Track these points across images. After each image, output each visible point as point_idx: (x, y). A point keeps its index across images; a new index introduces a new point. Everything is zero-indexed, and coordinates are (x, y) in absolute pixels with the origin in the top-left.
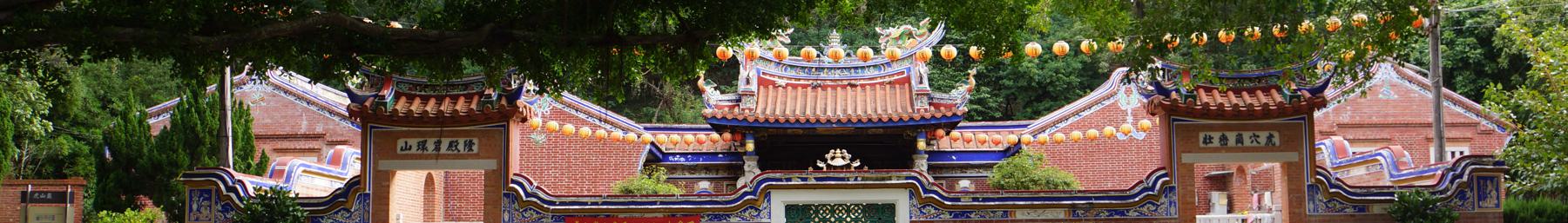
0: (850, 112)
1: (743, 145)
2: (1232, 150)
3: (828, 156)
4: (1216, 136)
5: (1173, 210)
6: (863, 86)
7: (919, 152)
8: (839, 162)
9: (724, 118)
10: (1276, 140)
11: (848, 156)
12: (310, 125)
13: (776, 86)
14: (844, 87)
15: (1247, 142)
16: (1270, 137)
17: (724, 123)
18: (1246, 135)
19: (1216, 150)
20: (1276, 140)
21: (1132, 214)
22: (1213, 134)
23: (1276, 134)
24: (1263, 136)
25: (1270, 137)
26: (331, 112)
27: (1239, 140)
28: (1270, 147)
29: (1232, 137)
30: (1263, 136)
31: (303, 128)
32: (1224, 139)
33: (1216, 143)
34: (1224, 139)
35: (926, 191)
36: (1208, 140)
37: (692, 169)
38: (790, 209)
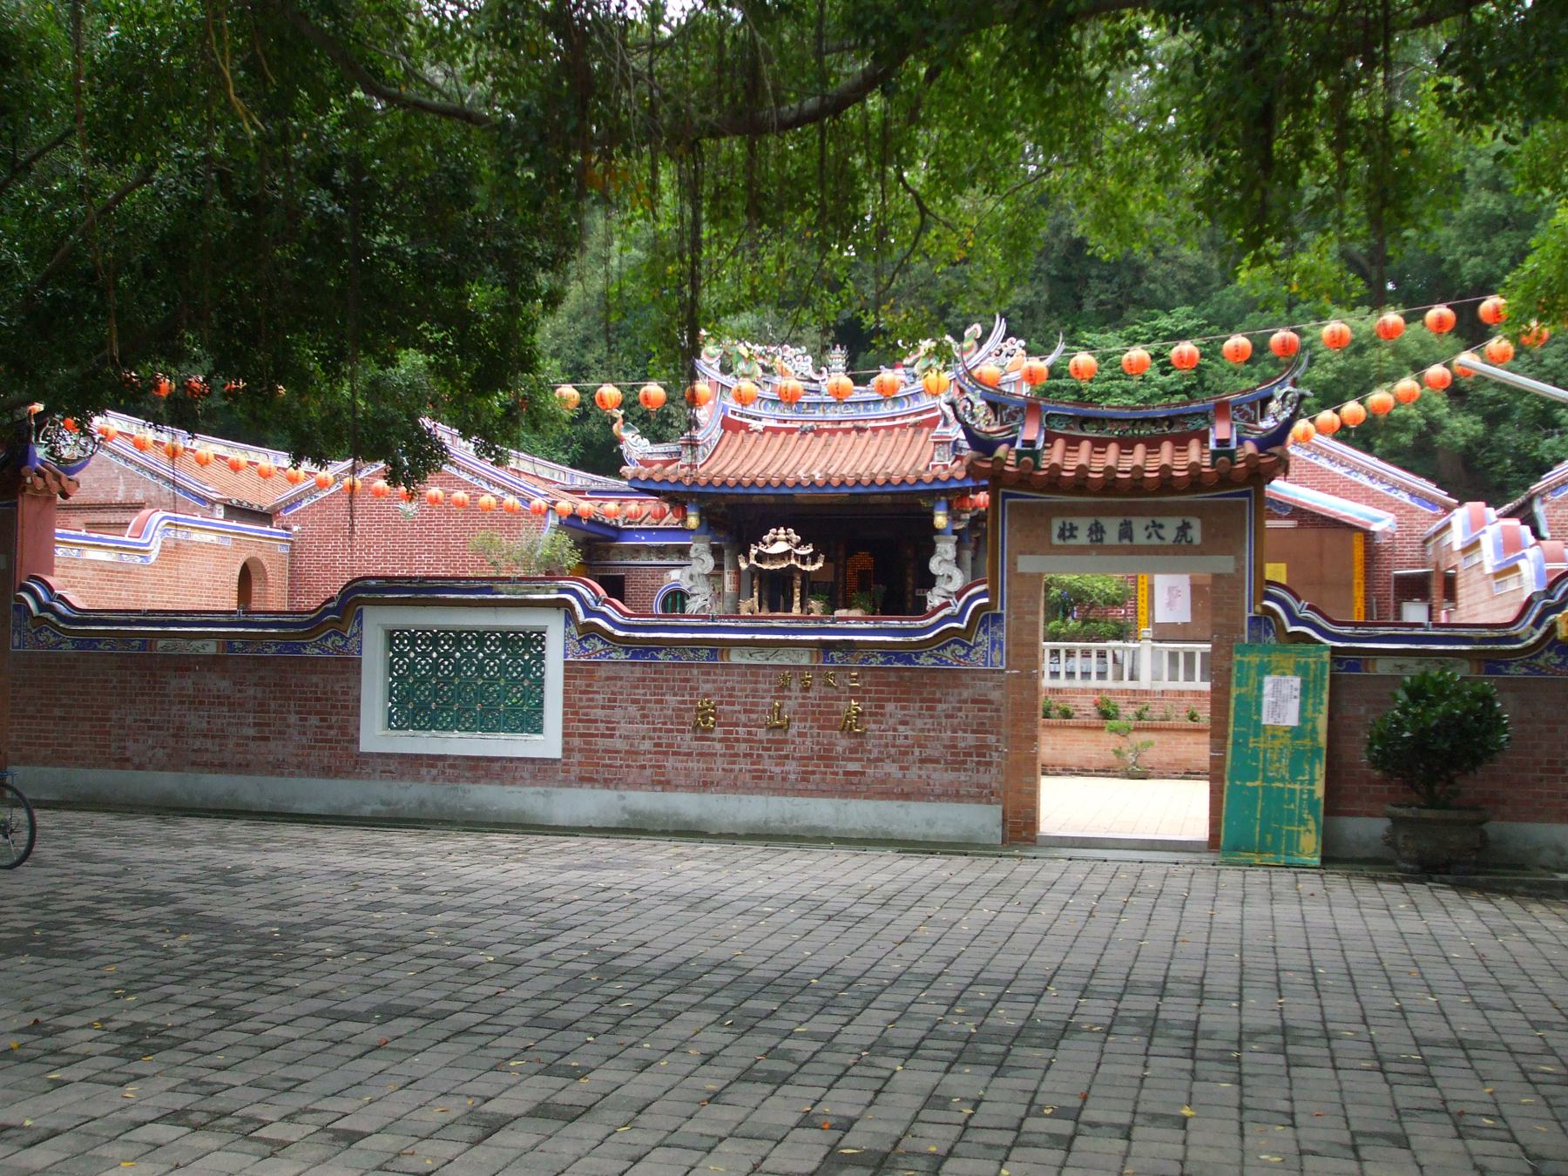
0: (801, 473)
1: (684, 520)
2: (1112, 550)
3: (767, 538)
4: (1083, 525)
5: (997, 656)
6: (875, 430)
7: (937, 532)
8: (780, 547)
9: (936, 479)
10: (1195, 534)
11: (796, 538)
12: (128, 490)
13: (749, 432)
14: (847, 431)
15: (1140, 537)
16: (1185, 527)
17: (937, 486)
18: (1139, 525)
19: (1081, 550)
20: (1195, 534)
21: (926, 661)
22: (1076, 521)
23: (1196, 523)
24: (1170, 526)
25: (1185, 527)
26: (153, 473)
27: (1126, 532)
28: (1181, 547)
29: (1112, 527)
30: (1170, 526)
31: (120, 497)
32: (1097, 530)
33: (1082, 538)
34: (1097, 530)
35: (589, 612)
36: (1068, 532)
37: (661, 551)
38: (391, 636)
